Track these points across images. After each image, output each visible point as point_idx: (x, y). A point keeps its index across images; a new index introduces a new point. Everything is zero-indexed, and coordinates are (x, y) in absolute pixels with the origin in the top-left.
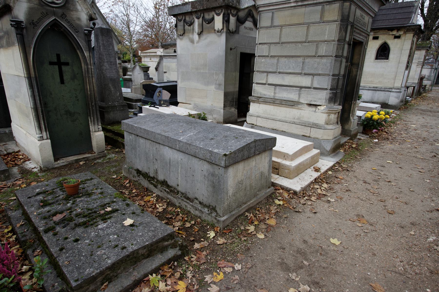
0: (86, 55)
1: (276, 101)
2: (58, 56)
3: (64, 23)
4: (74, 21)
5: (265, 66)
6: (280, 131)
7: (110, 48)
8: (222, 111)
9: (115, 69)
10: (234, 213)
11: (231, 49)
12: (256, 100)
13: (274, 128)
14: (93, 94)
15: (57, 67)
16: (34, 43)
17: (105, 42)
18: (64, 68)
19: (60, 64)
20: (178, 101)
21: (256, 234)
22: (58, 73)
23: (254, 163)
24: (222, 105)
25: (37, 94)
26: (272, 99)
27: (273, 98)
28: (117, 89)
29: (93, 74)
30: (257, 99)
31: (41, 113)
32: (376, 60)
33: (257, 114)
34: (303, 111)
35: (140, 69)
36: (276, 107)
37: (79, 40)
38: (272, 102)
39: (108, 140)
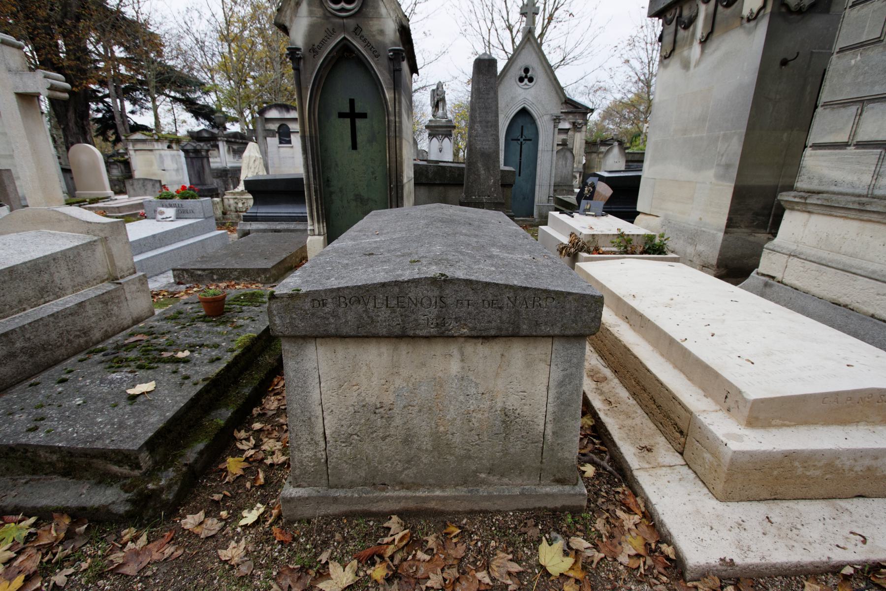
1: (870, 203)
2: (352, 102)
3: (358, 42)
4: (374, 36)
5: (860, 79)
6: (864, 314)
7: (489, 97)
8: (721, 235)
10: (339, 493)
11: (784, 63)
12: (797, 200)
13: (843, 300)
14: (393, 169)
15: (348, 121)
17: (481, 85)
18: (359, 122)
19: (353, 115)
22: (349, 130)
23: (455, 367)
24: (724, 221)
25: (310, 162)
26: (859, 196)
27: (865, 192)
28: (491, 172)
30: (801, 197)
33: (794, 247)
36: (869, 226)
37: (378, 69)
38: (856, 206)
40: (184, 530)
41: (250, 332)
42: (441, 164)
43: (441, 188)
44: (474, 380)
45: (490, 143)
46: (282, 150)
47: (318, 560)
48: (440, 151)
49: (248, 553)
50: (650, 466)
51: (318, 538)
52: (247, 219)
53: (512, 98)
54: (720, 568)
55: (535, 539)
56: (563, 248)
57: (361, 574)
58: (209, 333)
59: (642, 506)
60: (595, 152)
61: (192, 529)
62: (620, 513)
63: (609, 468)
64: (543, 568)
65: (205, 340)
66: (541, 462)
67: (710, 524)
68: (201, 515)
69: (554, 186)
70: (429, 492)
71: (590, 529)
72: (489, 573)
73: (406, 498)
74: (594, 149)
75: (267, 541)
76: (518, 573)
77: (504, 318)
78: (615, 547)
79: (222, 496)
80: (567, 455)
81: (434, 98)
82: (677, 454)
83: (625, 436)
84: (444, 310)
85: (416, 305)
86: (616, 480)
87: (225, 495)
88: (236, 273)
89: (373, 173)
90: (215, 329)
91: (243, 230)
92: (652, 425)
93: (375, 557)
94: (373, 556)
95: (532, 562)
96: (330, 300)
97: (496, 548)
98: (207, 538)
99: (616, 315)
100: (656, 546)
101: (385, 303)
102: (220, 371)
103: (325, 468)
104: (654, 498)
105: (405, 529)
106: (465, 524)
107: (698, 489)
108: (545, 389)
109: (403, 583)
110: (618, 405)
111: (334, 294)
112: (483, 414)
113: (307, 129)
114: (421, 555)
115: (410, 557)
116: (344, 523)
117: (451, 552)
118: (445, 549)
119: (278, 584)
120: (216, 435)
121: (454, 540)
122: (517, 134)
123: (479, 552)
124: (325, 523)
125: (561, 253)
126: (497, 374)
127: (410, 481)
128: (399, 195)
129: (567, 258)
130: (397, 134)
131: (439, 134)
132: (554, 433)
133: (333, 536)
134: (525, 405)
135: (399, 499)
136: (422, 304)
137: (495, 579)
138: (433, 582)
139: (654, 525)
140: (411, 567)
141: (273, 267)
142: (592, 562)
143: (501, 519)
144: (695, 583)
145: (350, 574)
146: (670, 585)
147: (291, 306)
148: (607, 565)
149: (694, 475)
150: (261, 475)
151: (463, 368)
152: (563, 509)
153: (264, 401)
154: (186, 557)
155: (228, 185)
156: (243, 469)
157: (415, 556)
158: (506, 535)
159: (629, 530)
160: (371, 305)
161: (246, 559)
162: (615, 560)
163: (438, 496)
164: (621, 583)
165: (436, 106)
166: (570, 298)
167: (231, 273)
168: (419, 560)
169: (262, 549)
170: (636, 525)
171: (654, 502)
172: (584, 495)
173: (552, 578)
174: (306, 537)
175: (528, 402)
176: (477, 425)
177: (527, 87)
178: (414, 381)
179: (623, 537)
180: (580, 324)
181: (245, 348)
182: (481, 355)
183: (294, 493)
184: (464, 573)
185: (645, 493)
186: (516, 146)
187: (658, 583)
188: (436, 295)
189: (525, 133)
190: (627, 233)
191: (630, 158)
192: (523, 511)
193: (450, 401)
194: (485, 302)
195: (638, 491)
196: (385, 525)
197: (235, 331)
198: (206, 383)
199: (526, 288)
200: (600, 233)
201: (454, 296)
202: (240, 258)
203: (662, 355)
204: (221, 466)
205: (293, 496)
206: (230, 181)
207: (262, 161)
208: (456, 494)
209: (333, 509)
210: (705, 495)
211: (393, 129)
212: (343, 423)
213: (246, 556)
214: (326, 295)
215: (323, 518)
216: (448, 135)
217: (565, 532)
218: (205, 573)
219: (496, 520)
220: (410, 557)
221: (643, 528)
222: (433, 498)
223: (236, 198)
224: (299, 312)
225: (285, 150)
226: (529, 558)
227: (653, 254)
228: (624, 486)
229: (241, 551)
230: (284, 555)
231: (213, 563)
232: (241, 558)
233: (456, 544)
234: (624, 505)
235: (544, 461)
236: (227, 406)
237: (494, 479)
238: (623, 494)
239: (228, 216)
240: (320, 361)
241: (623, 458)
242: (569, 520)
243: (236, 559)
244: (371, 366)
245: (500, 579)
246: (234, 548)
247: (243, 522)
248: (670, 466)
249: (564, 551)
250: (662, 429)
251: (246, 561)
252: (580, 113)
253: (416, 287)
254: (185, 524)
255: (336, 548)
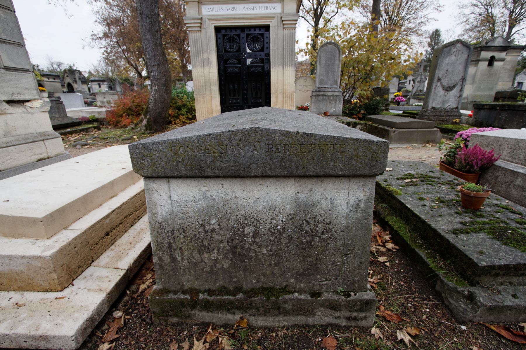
32: (225, 114)
34: (8, 115)
39: (155, 284)
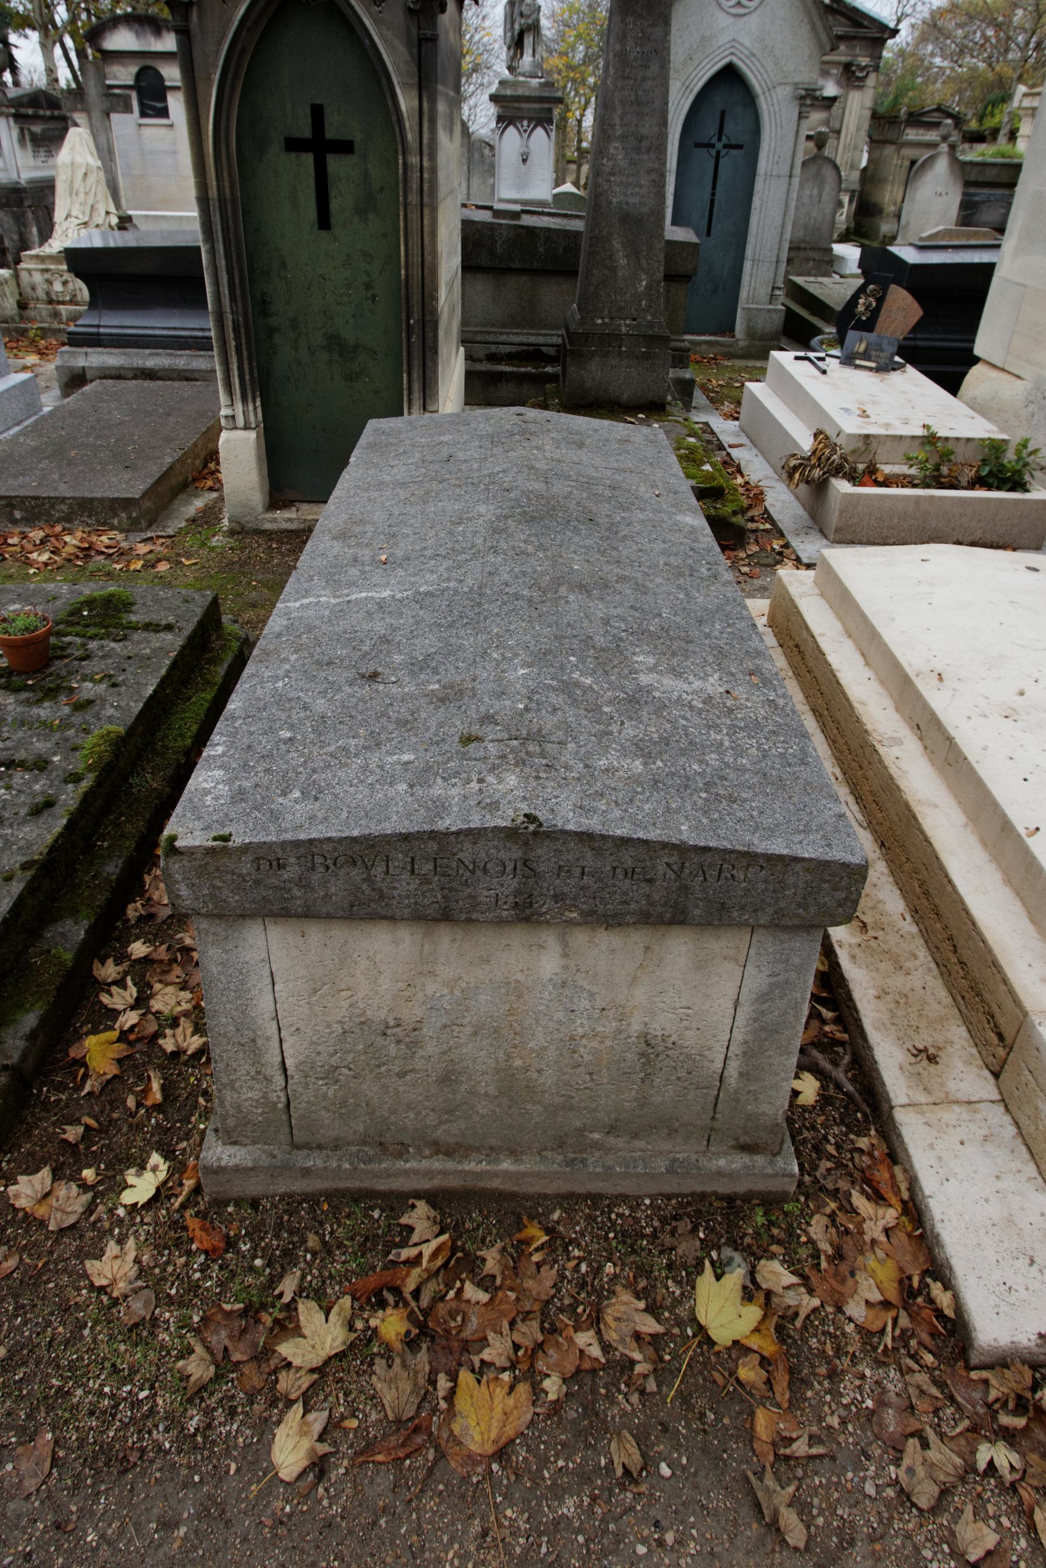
0: (403, 107)
2: (318, 113)
9: (649, 171)
14: (416, 281)
15: (308, 159)
16: (221, 62)
17: (630, 44)
18: (335, 164)
20: (978, 351)
21: (290, 1403)
22: (312, 182)
28: (644, 262)
29: (425, 193)
31: (232, 336)
35: (952, 172)
37: (382, 37)
40: (16, 1210)
41: (110, 719)
42: (527, 220)
43: (524, 280)
44: (586, 985)
45: (644, 191)
46: (147, 132)
47: (277, 1292)
48: (524, 161)
49: (143, 1272)
50: (931, 1100)
51: (275, 1243)
52: (78, 340)
53: (703, 38)
54: (1036, 1350)
55: (691, 1261)
56: (795, 468)
57: (359, 1325)
58: (22, 724)
59: (903, 1186)
60: (892, 143)
61: (32, 1208)
62: (858, 1200)
63: (849, 1087)
64: (701, 1329)
65: (16, 748)
66: (713, 1118)
67: (1030, 1253)
68: (45, 1174)
69: (790, 249)
70: (489, 1163)
71: (799, 1236)
72: (599, 1332)
73: (444, 1173)
74: (891, 135)
75: (178, 1243)
76: (654, 1336)
77: (656, 897)
78: (843, 1281)
79: (81, 1129)
80: (764, 1108)
81: (513, 22)
82: (986, 1073)
83: (885, 1017)
84: (531, 881)
85: (473, 872)
86: (859, 1115)
87: (87, 1127)
88: (64, 507)
89: (368, 286)
90: (35, 711)
91: (71, 369)
92: (943, 994)
93: (385, 1293)
94: (381, 1290)
95: (682, 1312)
96: (292, 860)
97: (616, 1276)
98: (62, 1231)
99: (897, 711)
100: (921, 1281)
101: (409, 867)
102: (56, 841)
103: (284, 1117)
104: (928, 1183)
105: (441, 1233)
106: (558, 1222)
107: (1016, 1165)
108: (730, 1004)
109: (437, 1348)
110: (880, 934)
111: (302, 850)
112: (601, 1042)
113: (213, 183)
114: (473, 1293)
115: (452, 1294)
116: (323, 1212)
117: (529, 1284)
118: (517, 1275)
119: (203, 1341)
120: (58, 989)
121: (536, 1258)
122: (709, 132)
123: (582, 1285)
124: (286, 1211)
125: (791, 476)
126: (635, 978)
127: (452, 1140)
128: (429, 343)
129: (803, 486)
130: (426, 199)
131: (522, 119)
132: (741, 1074)
133: (304, 1241)
134: (687, 1029)
135: (429, 1174)
136: (485, 870)
137: (610, 1346)
138: (494, 1352)
139: (922, 1236)
140: (453, 1316)
141: (146, 494)
142: (796, 1314)
143: (627, 1213)
144: (985, 1374)
145: (339, 1329)
146: (937, 1373)
147: (211, 868)
148: (823, 1322)
149: (1012, 1130)
150: (156, 1086)
151: (566, 968)
152: (748, 1197)
153: (147, 879)
154: (26, 1271)
155: (25, 225)
156: (119, 1061)
157: (460, 1291)
158: (634, 1251)
159: (873, 1242)
160: (379, 870)
161: (140, 1283)
162: (840, 1310)
163: (506, 1172)
164: (846, 1361)
165: (517, 44)
166: (798, 867)
167: (53, 506)
168: (468, 1301)
169: (168, 1263)
170: (887, 1231)
171: (927, 1192)
172: (793, 1176)
173: (717, 1348)
174: (252, 1240)
175: (694, 1025)
176: (587, 1058)
177: (742, 11)
178: (464, 985)
179: (860, 1258)
180: (813, 910)
181: (103, 770)
182: (604, 947)
183: (225, 1157)
184: (554, 1330)
185: (912, 1166)
186: (704, 160)
187: (916, 1367)
188: (515, 856)
189: (729, 128)
190: (942, 433)
191: (973, 177)
192: (669, 1197)
193: (537, 1021)
194: (618, 871)
195: (901, 1155)
196: (404, 1220)
197: (77, 719)
198: (29, 874)
199: (707, 849)
200: (882, 431)
201: (554, 860)
202: (71, 463)
203: (984, 843)
204: (74, 1053)
205: (223, 1163)
206: (30, 215)
207: (102, 174)
208: (543, 1168)
209: (300, 1186)
210: (1029, 1179)
211: (415, 186)
212: (320, 1048)
213: (139, 1277)
214: (284, 850)
215: (282, 1199)
216: (543, 120)
217: (749, 1246)
218: (66, 1310)
219: (618, 1215)
220: (452, 1294)
221: (900, 1238)
222: (496, 1175)
223: (47, 270)
224: (229, 877)
225: (154, 132)
226: (677, 1302)
227: (999, 488)
228: (873, 1132)
229: (127, 1268)
230: (211, 1278)
231: (78, 1289)
232: (130, 1283)
233: (539, 1265)
234: (868, 1181)
235: (718, 1116)
236: (74, 913)
237: (618, 1142)
238: (870, 1154)
239: (31, 313)
240: (273, 949)
241: (877, 1070)
242: (760, 1220)
243: (121, 1285)
244: (378, 960)
245: (620, 1348)
246: (116, 1257)
247: (128, 1197)
248: (969, 1103)
249: (745, 1288)
250: (963, 1008)
251: (141, 1288)
252: (864, 39)
253: (475, 843)
254: (17, 1196)
255: (310, 1265)
